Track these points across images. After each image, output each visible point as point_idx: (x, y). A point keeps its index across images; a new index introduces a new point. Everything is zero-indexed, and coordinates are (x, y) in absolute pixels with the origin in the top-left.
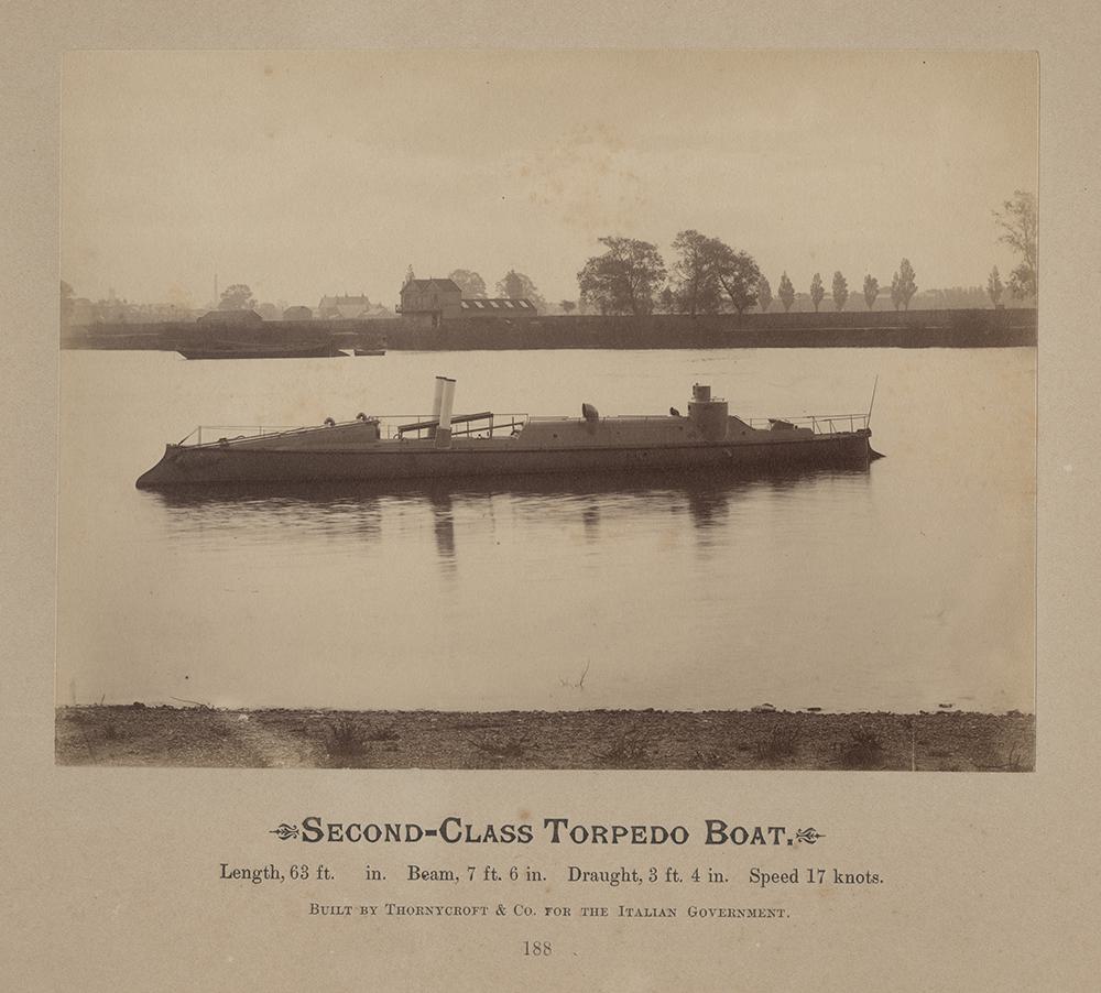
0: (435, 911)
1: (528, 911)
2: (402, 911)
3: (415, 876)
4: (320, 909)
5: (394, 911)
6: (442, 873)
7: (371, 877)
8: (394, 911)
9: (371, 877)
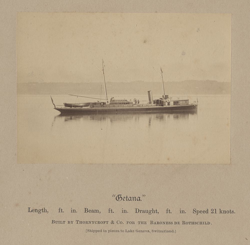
0: (92, 223)
1: (121, 223)
2: (81, 222)
3: (86, 211)
4: (55, 222)
5: (79, 222)
6: (95, 210)
7: (73, 212)
8: (79, 222)
9: (73, 212)
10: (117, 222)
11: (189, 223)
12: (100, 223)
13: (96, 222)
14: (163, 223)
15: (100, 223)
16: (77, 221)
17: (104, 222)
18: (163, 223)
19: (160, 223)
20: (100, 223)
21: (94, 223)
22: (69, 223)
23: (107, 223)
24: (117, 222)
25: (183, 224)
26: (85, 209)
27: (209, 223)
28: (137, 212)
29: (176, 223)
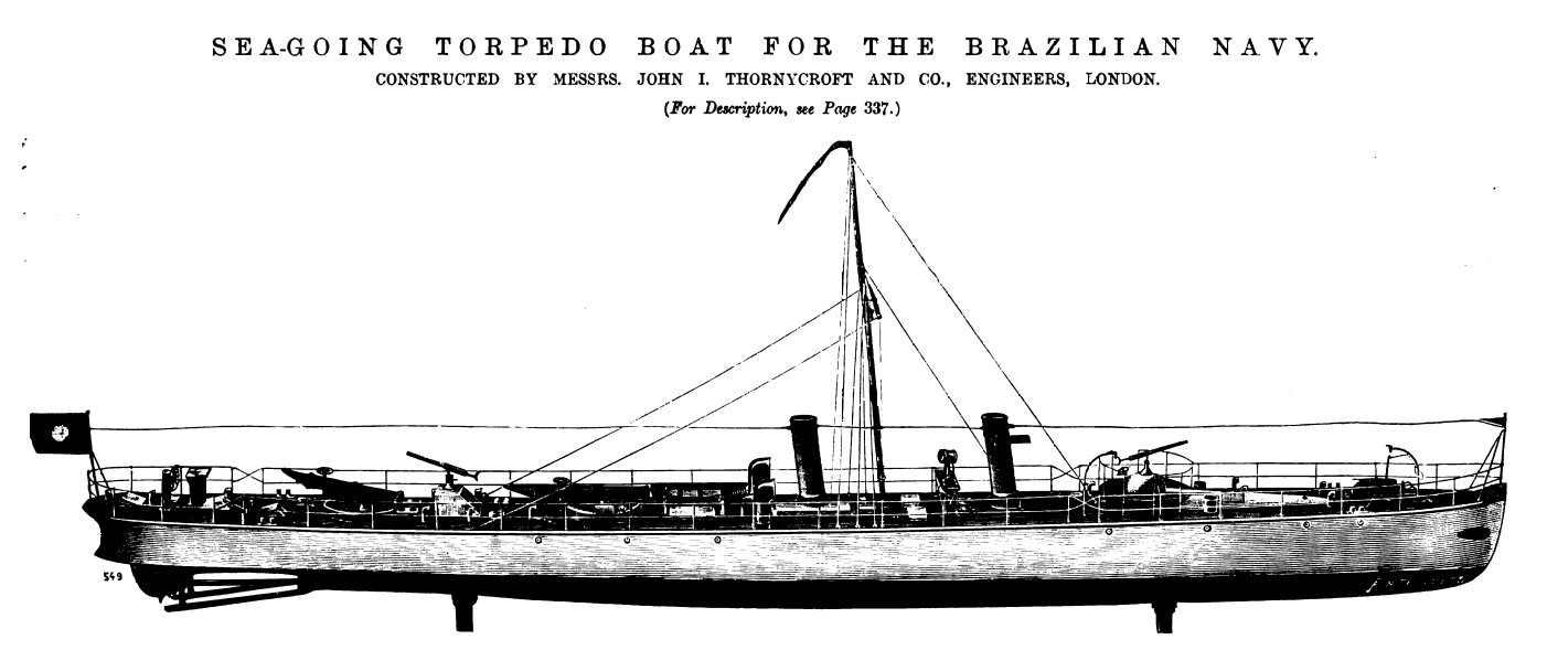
0: (786, 80)
5: (735, 80)
8: (735, 80)
10: (667, 42)
11: (420, 79)
12: (819, 79)
13: (804, 79)
14: (1144, 77)
15: (819, 79)
16: (721, 41)
17: (835, 75)
18: (1108, 81)
19: (1105, 79)
20: (440, 83)
21: (796, 80)
22: (975, 50)
23: (724, 53)
24: (667, 42)
25: (997, 53)
26: (819, 43)
27: (572, 48)
28: (570, 52)
29: (572, 45)
